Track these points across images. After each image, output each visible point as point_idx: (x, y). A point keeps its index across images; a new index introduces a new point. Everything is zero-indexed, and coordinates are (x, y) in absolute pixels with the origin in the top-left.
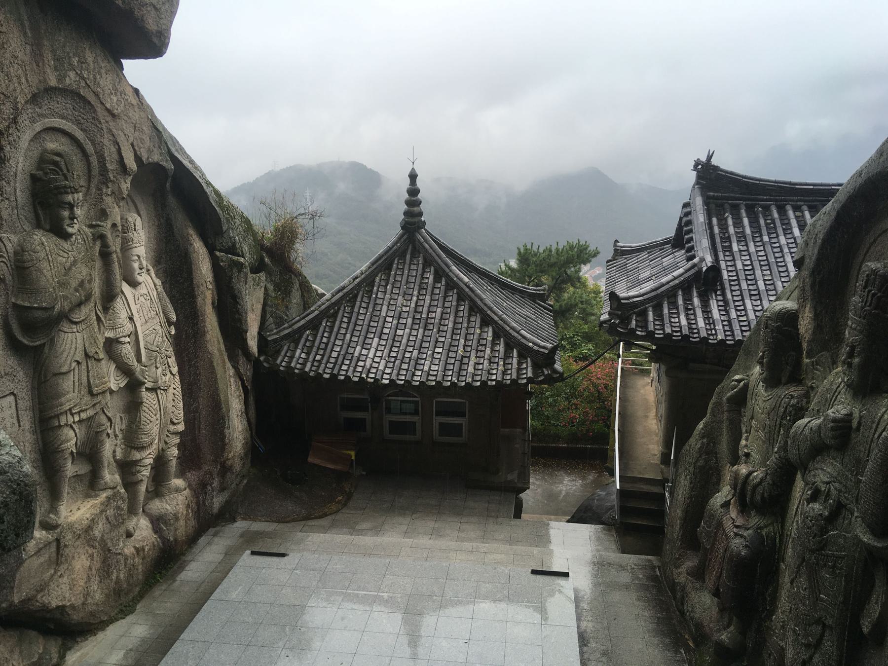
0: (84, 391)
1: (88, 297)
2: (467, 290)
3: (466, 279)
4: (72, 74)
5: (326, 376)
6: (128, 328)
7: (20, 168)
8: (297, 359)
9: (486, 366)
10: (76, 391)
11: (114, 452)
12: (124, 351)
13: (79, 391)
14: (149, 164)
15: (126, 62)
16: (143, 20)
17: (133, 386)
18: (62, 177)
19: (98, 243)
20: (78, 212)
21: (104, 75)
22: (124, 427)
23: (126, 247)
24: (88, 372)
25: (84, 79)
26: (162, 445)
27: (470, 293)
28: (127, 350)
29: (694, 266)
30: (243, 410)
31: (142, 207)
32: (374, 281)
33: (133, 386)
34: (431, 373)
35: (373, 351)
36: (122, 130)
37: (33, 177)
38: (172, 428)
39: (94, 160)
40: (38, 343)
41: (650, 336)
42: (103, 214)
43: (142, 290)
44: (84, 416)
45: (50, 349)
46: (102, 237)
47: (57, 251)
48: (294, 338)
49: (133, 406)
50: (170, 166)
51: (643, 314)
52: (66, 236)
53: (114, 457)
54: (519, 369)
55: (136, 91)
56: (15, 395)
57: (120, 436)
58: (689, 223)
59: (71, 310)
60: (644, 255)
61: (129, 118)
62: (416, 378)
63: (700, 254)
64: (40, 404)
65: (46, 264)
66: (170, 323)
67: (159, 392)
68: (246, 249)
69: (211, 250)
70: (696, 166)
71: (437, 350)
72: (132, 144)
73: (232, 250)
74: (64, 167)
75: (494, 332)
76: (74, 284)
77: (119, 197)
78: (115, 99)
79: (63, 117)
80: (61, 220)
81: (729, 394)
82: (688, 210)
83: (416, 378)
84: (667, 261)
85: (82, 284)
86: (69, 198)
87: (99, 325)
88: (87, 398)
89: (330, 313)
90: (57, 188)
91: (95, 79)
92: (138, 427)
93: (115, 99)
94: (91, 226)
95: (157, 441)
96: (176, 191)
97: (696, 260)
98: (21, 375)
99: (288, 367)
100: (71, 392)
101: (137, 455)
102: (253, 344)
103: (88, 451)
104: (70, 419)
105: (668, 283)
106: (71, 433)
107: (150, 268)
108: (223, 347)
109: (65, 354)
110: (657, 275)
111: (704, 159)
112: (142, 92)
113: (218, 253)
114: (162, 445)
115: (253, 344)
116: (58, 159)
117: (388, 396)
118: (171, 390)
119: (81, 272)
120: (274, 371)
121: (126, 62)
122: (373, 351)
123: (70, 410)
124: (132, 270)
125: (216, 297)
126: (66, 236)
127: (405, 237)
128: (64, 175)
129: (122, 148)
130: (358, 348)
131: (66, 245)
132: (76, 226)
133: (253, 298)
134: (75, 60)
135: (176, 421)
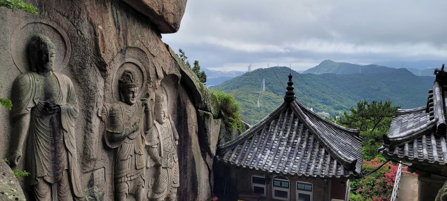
0: (133, 167)
1: (137, 129)
2: (313, 129)
3: (313, 125)
4: (138, 41)
5: (244, 167)
6: (157, 141)
7: (114, 78)
8: (232, 158)
9: (320, 167)
10: (130, 167)
11: (148, 194)
12: (154, 151)
13: (131, 168)
14: (170, 75)
15: (163, 35)
16: (167, 19)
17: (157, 167)
18: (130, 81)
19: (144, 107)
20: (136, 94)
21: (151, 41)
22: (153, 183)
23: (158, 107)
24: (135, 160)
25: (143, 43)
26: (169, 192)
27: (314, 132)
28: (155, 151)
29: (432, 123)
30: (208, 179)
31: (168, 92)
32: (270, 124)
33: (157, 167)
34: (293, 169)
35: (267, 156)
36: (158, 62)
37: (120, 82)
38: (173, 185)
39: (145, 74)
40: (116, 147)
41: (406, 159)
42: (148, 95)
43: (165, 125)
44: (132, 178)
45: (120, 150)
46: (146, 105)
47: (126, 110)
48: (232, 148)
49: (156, 176)
50: (179, 75)
51: (403, 147)
52: (131, 104)
53: (147, 196)
54: (337, 170)
55: (167, 46)
56: (105, 168)
57: (151, 187)
58: (432, 101)
59: (129, 134)
60: (412, 115)
61: (161, 57)
62: (285, 171)
63: (436, 117)
64: (115, 172)
65: (121, 115)
66: (176, 140)
67: (168, 169)
68: (212, 108)
69: (197, 108)
70: (435, 72)
71: (297, 158)
72: (162, 67)
73: (206, 109)
74: (131, 77)
75: (326, 151)
76: (132, 123)
77: (155, 88)
78: (155, 50)
79: (133, 58)
80: (129, 98)
81: (443, 195)
82: (432, 94)
83: (285, 171)
84: (422, 119)
85: (135, 124)
86: (133, 89)
87: (143, 140)
88: (134, 171)
89: (249, 138)
90: (129, 85)
91: (147, 42)
92: (158, 184)
93: (155, 50)
94: (142, 100)
95: (166, 190)
96: (185, 85)
97: (434, 120)
98: (108, 160)
99: (229, 162)
100: (127, 167)
101: (157, 196)
102: (213, 150)
103: (134, 193)
104: (126, 179)
105: (417, 132)
106: (126, 185)
107: (170, 116)
108: (199, 151)
109: (126, 152)
110: (416, 126)
111: (440, 68)
112: (170, 46)
113: (199, 110)
114: (169, 192)
115: (213, 150)
116: (129, 74)
117: (275, 178)
118: (174, 169)
119: (135, 119)
120: (222, 162)
121: (163, 35)
122: (267, 156)
123: (126, 175)
124: (161, 117)
125: (197, 127)
126: (131, 104)
127: (286, 104)
128: (131, 80)
129: (157, 69)
130: (260, 154)
131: (131, 108)
132: (135, 100)
133: (214, 129)
134: (139, 36)
135: (175, 182)
